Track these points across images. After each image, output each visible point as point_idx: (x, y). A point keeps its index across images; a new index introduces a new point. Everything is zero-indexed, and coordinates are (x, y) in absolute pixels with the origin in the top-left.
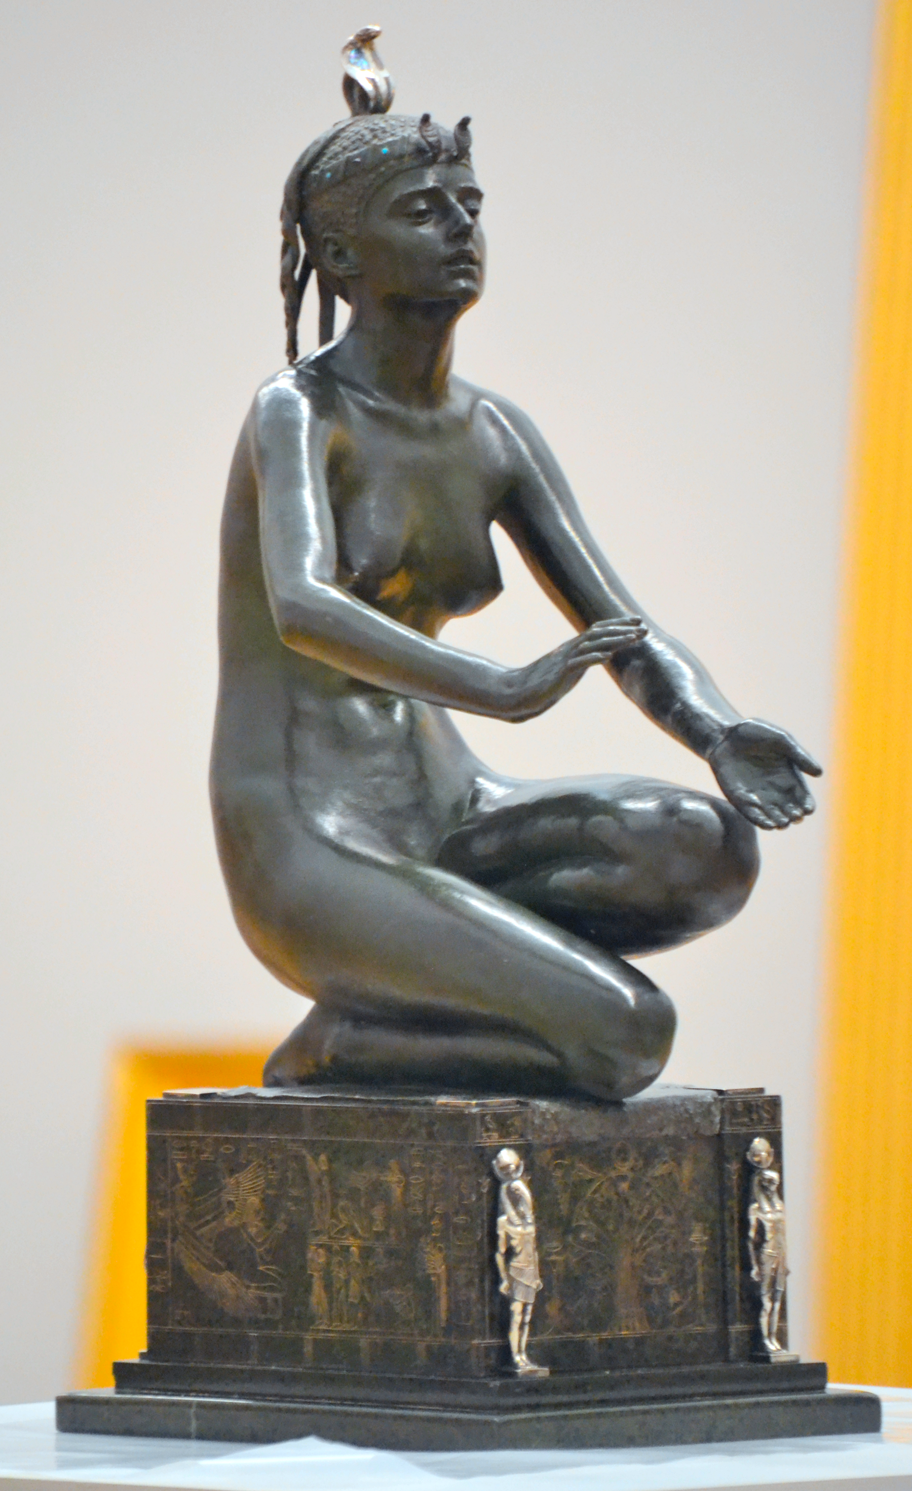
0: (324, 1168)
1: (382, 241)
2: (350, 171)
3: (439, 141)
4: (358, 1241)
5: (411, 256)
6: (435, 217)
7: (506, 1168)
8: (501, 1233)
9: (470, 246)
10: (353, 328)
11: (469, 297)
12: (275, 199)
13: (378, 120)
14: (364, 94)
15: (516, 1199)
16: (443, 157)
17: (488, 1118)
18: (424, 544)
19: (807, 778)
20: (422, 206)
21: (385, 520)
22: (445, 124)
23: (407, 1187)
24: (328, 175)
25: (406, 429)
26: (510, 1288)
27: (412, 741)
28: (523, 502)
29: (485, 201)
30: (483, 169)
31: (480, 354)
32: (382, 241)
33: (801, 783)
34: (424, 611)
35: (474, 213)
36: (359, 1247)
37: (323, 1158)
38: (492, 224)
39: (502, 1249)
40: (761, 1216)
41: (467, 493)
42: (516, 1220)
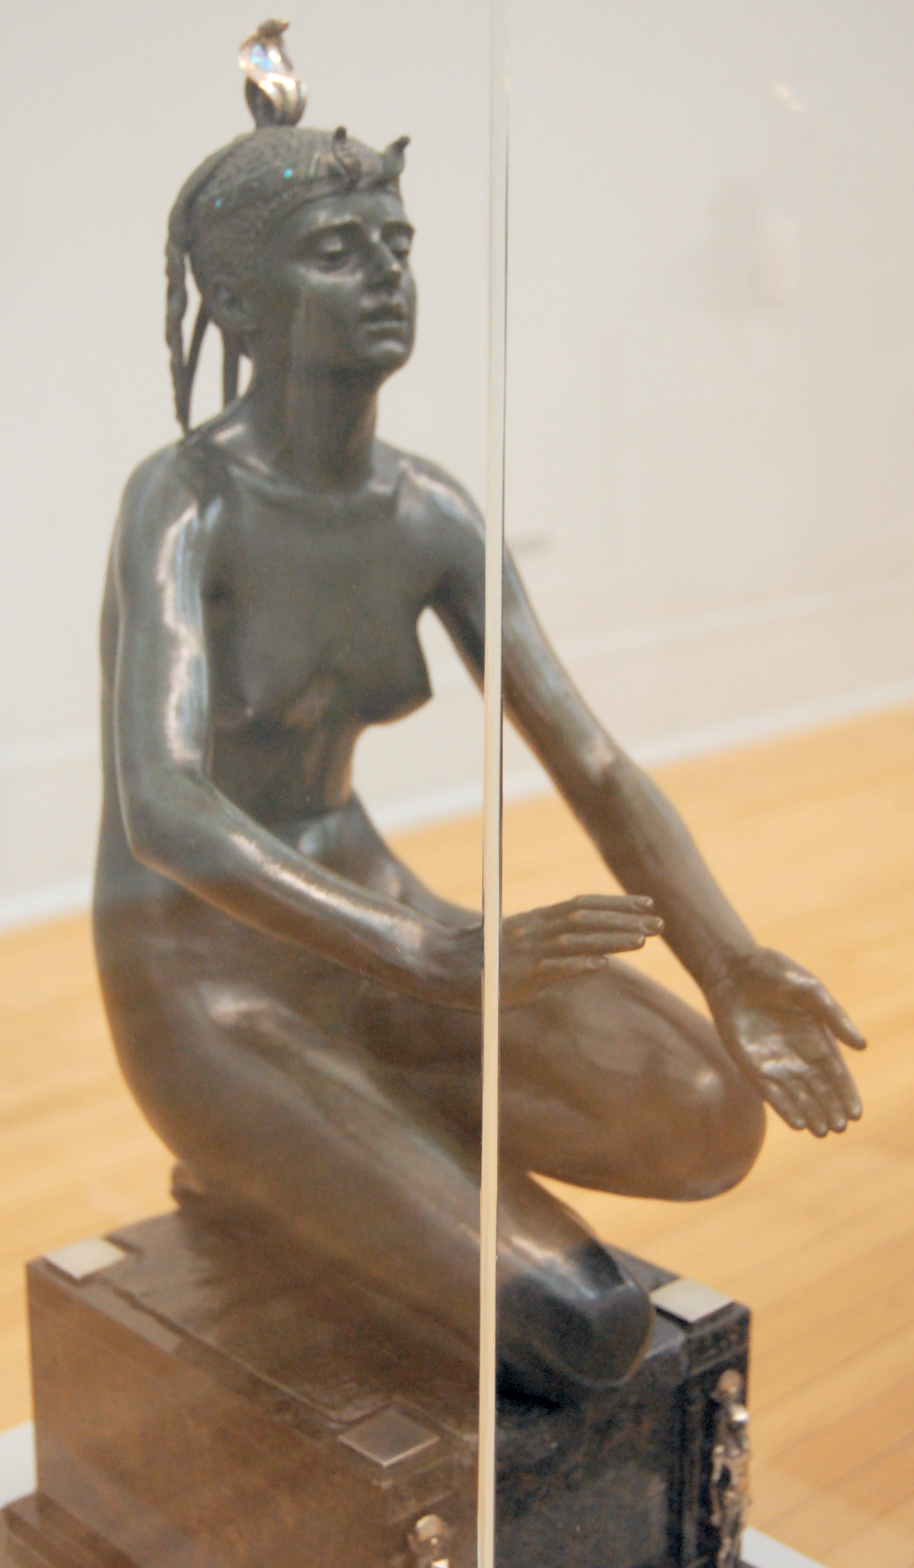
1: (292, 271)
2: (252, 195)
3: (358, 164)
6: (354, 259)
9: (397, 299)
11: (394, 363)
13: (283, 132)
14: (268, 103)
16: (363, 183)
19: (844, 1050)
20: (336, 246)
22: (373, 138)
24: (218, 203)
29: (417, 239)
31: (403, 415)
32: (292, 271)
33: (835, 1053)
35: (401, 255)
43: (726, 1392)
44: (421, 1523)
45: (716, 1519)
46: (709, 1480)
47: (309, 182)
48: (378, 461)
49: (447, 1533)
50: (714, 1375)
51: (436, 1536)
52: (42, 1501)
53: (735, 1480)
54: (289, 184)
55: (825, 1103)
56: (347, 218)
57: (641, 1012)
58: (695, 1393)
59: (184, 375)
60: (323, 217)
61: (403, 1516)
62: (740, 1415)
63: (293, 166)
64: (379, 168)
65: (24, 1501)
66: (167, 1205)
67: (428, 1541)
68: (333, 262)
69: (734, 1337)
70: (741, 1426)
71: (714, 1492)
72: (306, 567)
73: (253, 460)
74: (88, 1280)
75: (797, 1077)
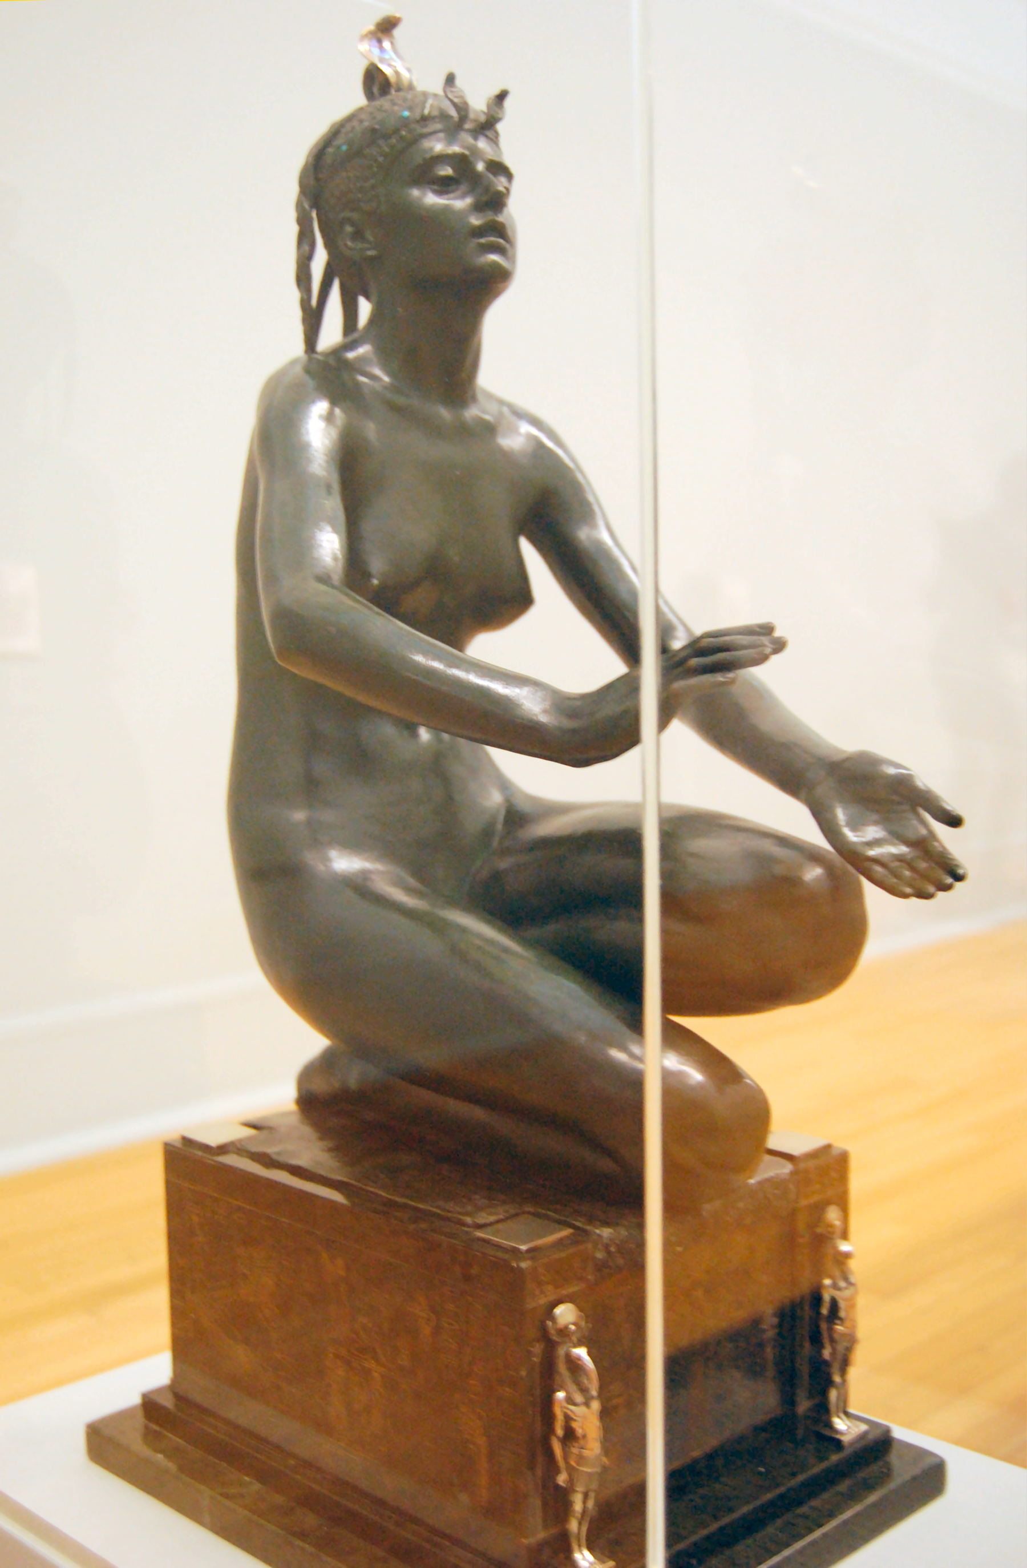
1: (405, 230)
2: (375, 135)
5: (435, 223)
6: (463, 187)
7: (564, 1332)
10: (372, 321)
15: (575, 1366)
16: (468, 126)
18: (454, 554)
20: (447, 171)
21: (409, 526)
23: (437, 1330)
25: (434, 430)
26: (571, 1481)
27: (437, 767)
28: (550, 511)
30: (512, 144)
32: (405, 230)
36: (383, 1376)
37: (340, 1262)
38: (520, 210)
39: (560, 1432)
42: (579, 1398)
44: (559, 1310)
45: (826, 1353)
46: (819, 1313)
47: (424, 119)
49: (583, 1324)
50: (819, 1208)
51: (574, 1324)
52: (174, 1388)
53: (842, 1314)
54: (405, 122)
55: (932, 873)
57: (740, 837)
58: (801, 1226)
60: (438, 147)
61: (543, 1301)
62: (844, 1247)
64: (483, 118)
65: (160, 1391)
66: (293, 1107)
67: (566, 1327)
68: (444, 186)
69: (834, 1174)
70: (847, 1255)
71: (824, 1326)
72: (410, 526)
73: (377, 371)
75: (900, 858)
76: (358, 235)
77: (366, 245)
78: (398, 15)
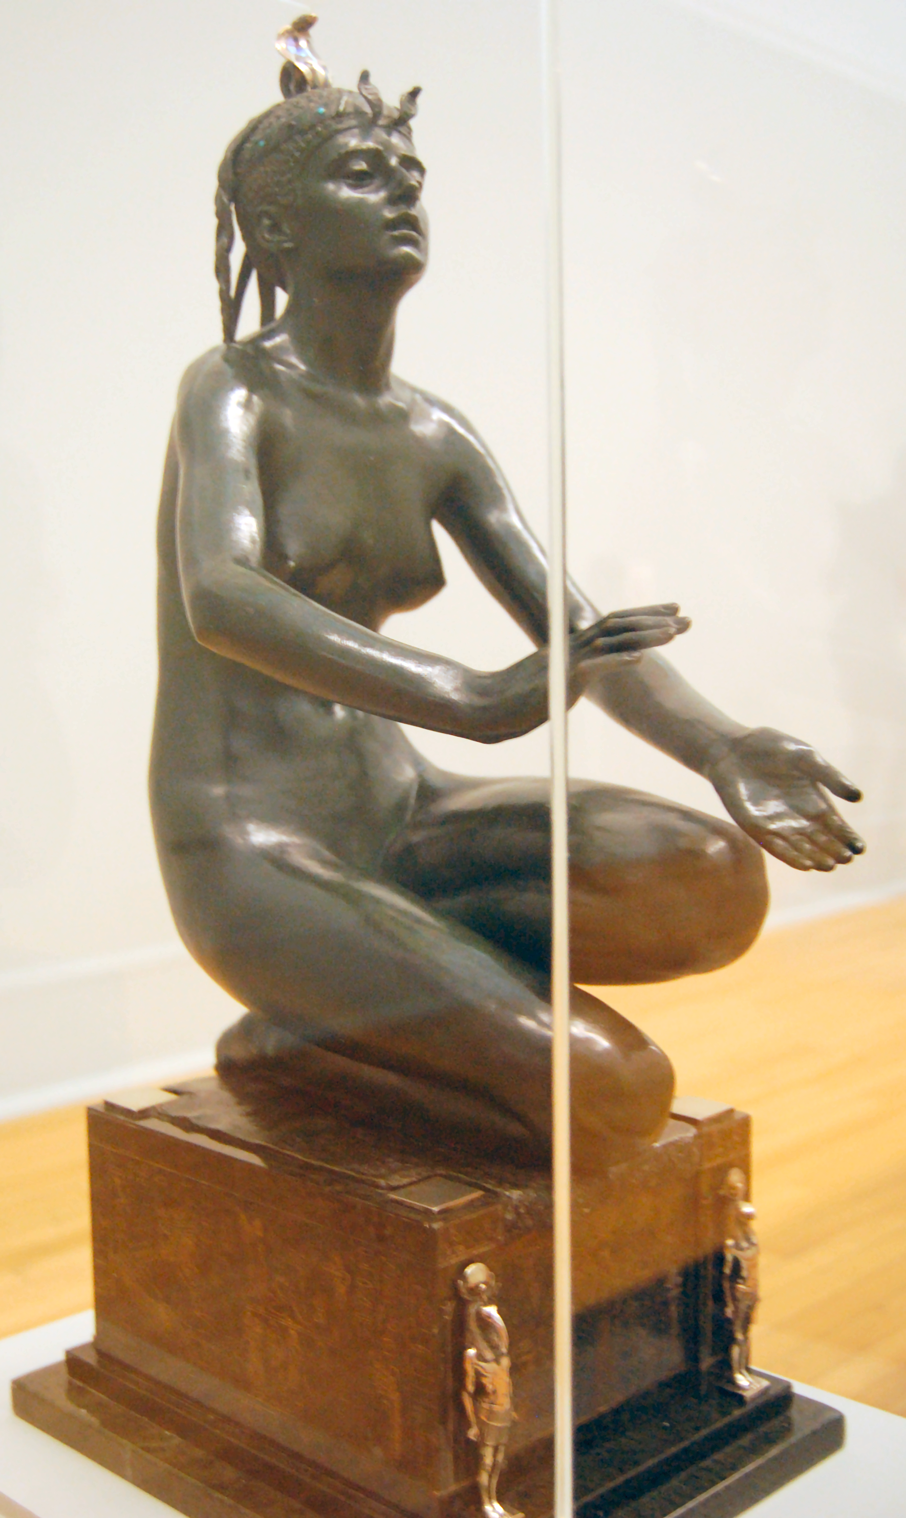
0: (260, 1234)
1: (320, 220)
2: (292, 130)
4: (299, 1327)
6: (377, 182)
7: (474, 1291)
8: (469, 1368)
10: (289, 311)
12: (209, 185)
15: (485, 1323)
16: (381, 122)
17: (453, 1231)
18: (368, 537)
20: (362, 166)
21: (325, 509)
23: (352, 1289)
25: (349, 416)
26: (481, 1435)
28: (461, 495)
30: (426, 139)
32: (320, 220)
34: (366, 608)
39: (471, 1388)
40: (739, 1254)
41: (411, 489)
42: (489, 1355)
43: (733, 1188)
44: (470, 1270)
45: (729, 1311)
46: (721, 1273)
47: (339, 116)
48: (388, 387)
49: (493, 1283)
51: (484, 1283)
52: (97, 1345)
53: (744, 1273)
54: (321, 119)
56: (370, 144)
58: (705, 1188)
59: (231, 310)
60: (353, 142)
61: (454, 1261)
62: (746, 1208)
63: (326, 105)
64: (396, 115)
65: (83, 1348)
67: (477, 1286)
68: (359, 180)
70: (749, 1217)
71: (726, 1285)
72: (324, 504)
73: (294, 360)
74: (144, 1114)
75: (800, 832)
76: (275, 228)
77: (283, 238)
78: (314, 15)
